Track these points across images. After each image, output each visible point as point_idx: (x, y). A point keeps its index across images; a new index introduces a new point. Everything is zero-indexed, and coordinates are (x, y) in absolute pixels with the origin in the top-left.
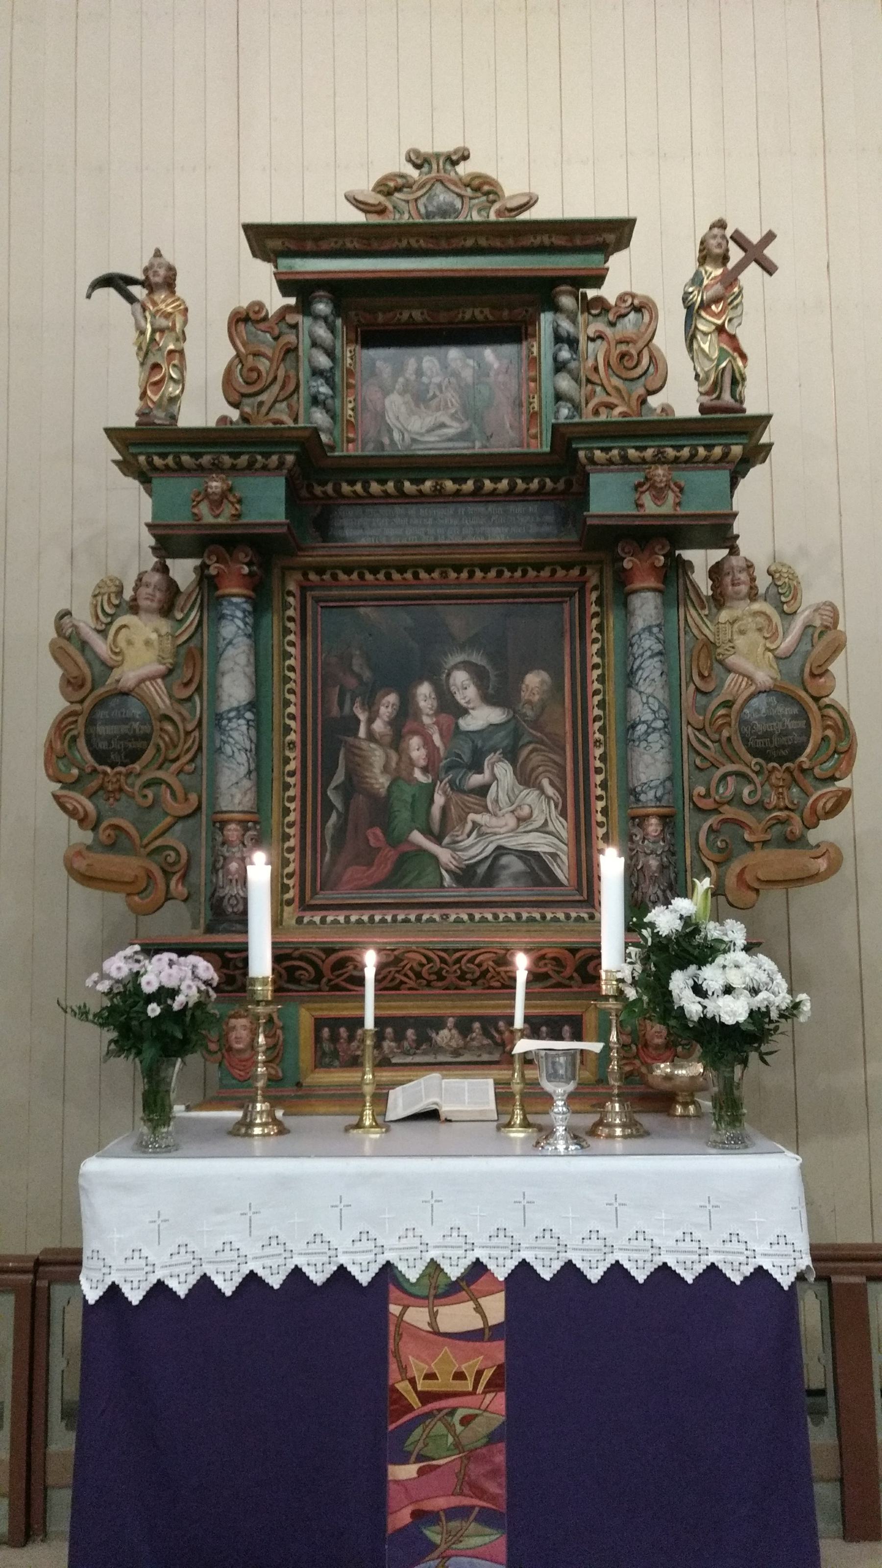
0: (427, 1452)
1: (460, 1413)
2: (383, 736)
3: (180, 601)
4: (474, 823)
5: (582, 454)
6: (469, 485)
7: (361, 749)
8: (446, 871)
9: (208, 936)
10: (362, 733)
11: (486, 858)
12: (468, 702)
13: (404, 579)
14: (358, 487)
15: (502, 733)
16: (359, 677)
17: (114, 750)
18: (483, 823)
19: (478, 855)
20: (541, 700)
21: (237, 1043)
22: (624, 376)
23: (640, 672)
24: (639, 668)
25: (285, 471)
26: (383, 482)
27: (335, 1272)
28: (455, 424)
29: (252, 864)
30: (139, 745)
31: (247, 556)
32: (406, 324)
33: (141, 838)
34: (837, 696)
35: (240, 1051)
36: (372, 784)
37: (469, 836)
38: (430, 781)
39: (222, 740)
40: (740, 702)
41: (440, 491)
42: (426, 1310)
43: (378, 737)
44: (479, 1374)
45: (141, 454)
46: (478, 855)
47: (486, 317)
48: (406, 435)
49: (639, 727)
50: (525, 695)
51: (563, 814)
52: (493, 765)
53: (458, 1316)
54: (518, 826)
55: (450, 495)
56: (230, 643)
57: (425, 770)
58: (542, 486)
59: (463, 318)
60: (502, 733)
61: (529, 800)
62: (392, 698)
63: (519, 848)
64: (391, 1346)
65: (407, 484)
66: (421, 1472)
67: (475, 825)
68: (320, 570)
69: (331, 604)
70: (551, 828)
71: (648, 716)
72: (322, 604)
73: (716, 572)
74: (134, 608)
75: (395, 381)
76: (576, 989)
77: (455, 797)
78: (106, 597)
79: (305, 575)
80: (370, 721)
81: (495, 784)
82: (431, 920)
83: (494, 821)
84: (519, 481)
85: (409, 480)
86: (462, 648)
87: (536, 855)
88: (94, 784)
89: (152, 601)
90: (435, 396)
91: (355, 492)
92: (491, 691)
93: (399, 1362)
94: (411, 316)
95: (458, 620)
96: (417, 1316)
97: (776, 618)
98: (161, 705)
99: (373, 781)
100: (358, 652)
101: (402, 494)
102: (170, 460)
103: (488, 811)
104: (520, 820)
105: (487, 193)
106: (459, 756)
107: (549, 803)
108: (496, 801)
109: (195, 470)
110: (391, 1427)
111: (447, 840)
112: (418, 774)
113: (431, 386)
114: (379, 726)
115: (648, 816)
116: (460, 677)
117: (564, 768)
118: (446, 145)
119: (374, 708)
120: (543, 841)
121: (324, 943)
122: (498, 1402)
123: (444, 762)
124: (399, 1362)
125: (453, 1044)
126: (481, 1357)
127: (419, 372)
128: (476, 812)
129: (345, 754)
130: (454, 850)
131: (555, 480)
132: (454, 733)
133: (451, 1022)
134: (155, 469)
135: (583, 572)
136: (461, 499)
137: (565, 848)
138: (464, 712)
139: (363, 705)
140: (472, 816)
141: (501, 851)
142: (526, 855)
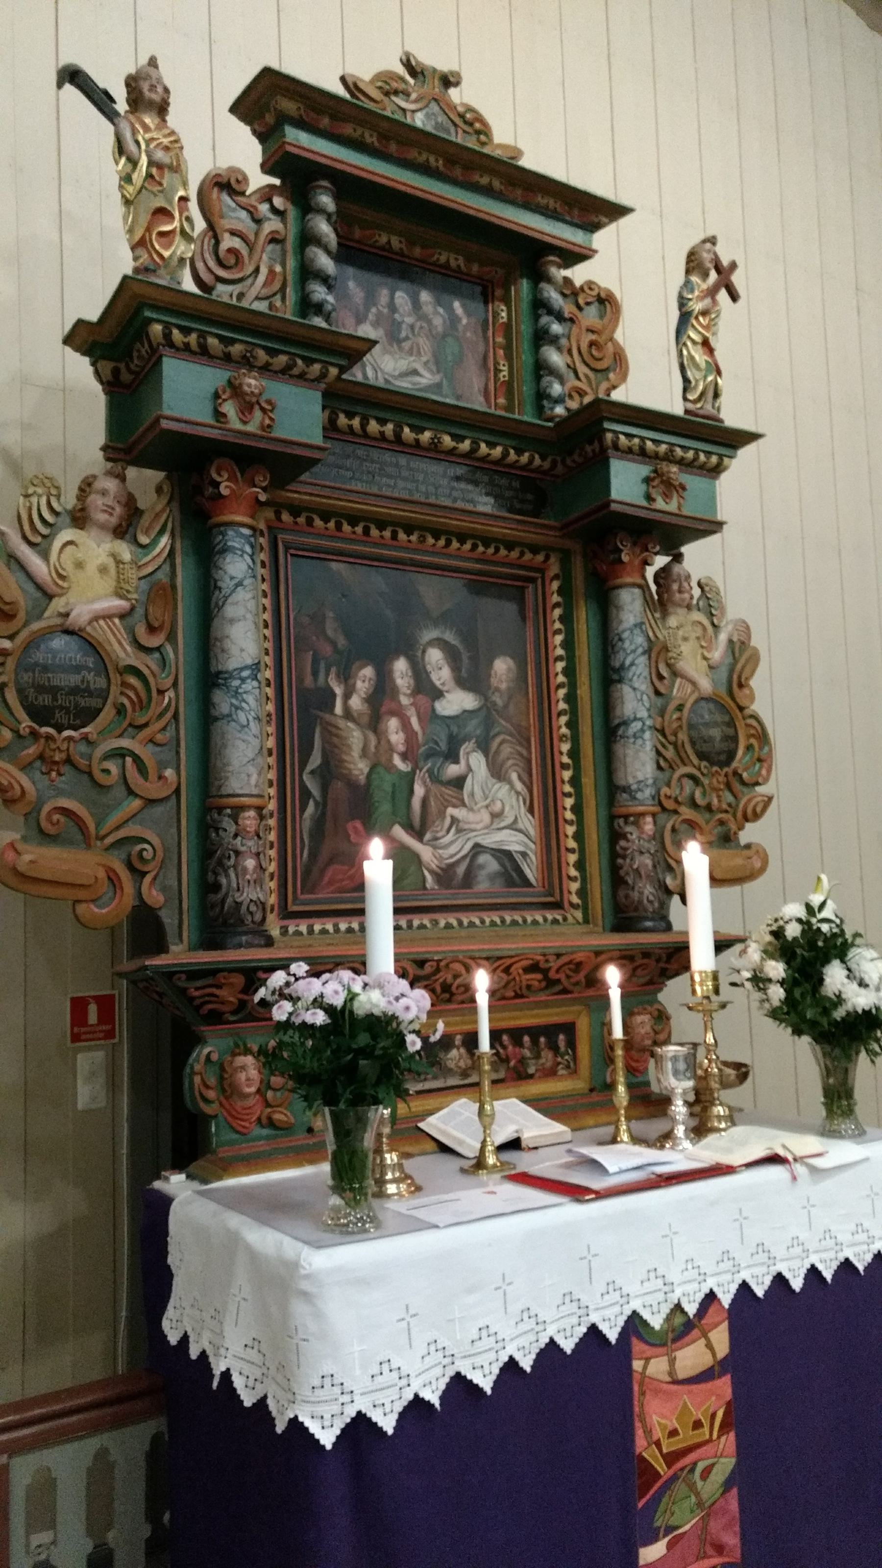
0: (673, 1522)
1: (701, 1466)
2: (360, 714)
3: (145, 521)
4: (452, 817)
5: (609, 436)
6: (466, 445)
7: (338, 728)
8: (428, 869)
9: (192, 954)
10: (338, 709)
11: (464, 858)
12: (443, 684)
13: (382, 537)
14: (356, 422)
15: (474, 722)
16: (334, 644)
17: (61, 708)
18: (460, 818)
19: (455, 854)
20: (509, 688)
21: (248, 1086)
22: (593, 366)
23: (634, 668)
24: (632, 664)
25: (323, 386)
26: (382, 422)
27: (585, 1335)
28: (427, 374)
29: (368, 858)
30: (94, 702)
31: (265, 480)
32: (382, 248)
33: (97, 825)
34: (759, 707)
35: (248, 1095)
36: (350, 770)
37: (448, 831)
38: (409, 769)
39: (232, 705)
40: (688, 705)
41: (436, 446)
42: (666, 1358)
43: (355, 715)
44: (713, 1416)
45: (158, 321)
46: (455, 854)
47: (459, 266)
48: (379, 374)
49: (633, 725)
50: (494, 682)
51: (531, 810)
52: (468, 754)
53: (692, 1357)
54: (492, 823)
55: (443, 452)
56: (240, 584)
57: (404, 756)
58: (531, 460)
59: (438, 259)
60: (474, 722)
61: (500, 795)
62: (368, 672)
63: (493, 846)
64: (637, 1409)
65: (407, 430)
66: (670, 1546)
67: (454, 820)
68: (295, 511)
69: (300, 553)
70: (520, 825)
71: (643, 714)
72: (292, 551)
73: (663, 576)
74: (79, 518)
75: (367, 310)
76: (575, 995)
77: (435, 789)
78: (44, 500)
79: (278, 514)
80: (347, 696)
81: (470, 776)
82: (422, 927)
83: (471, 817)
84: (512, 451)
85: (410, 426)
86: (436, 624)
87: (508, 854)
88: (32, 750)
89: (111, 514)
90: (407, 338)
91: (351, 427)
92: (464, 673)
93: (644, 1426)
94: (389, 242)
95: (432, 591)
96: (658, 1367)
97: (710, 628)
98: (122, 655)
99: (352, 766)
100: (331, 614)
101: (398, 438)
102: (193, 338)
103: (464, 805)
104: (495, 816)
105: (478, 132)
106: (436, 743)
107: (518, 800)
108: (472, 794)
109: (220, 359)
110: (640, 1505)
111: (428, 836)
112: (397, 761)
113: (404, 326)
114: (356, 702)
115: (643, 814)
116: (435, 655)
117: (529, 761)
118: (444, 65)
119: (351, 681)
120: (514, 839)
121: (417, 953)
122: (729, 1442)
123: (423, 748)
124: (644, 1426)
125: (462, 1064)
126: (714, 1398)
127: (393, 307)
128: (455, 806)
129: (321, 733)
130: (435, 848)
131: (543, 458)
132: (430, 717)
133: (458, 1039)
134: (171, 344)
135: (547, 557)
136: (453, 459)
137: (533, 846)
138: (438, 694)
139: (338, 676)
140: (450, 811)
141: (478, 849)
142: (503, 855)
